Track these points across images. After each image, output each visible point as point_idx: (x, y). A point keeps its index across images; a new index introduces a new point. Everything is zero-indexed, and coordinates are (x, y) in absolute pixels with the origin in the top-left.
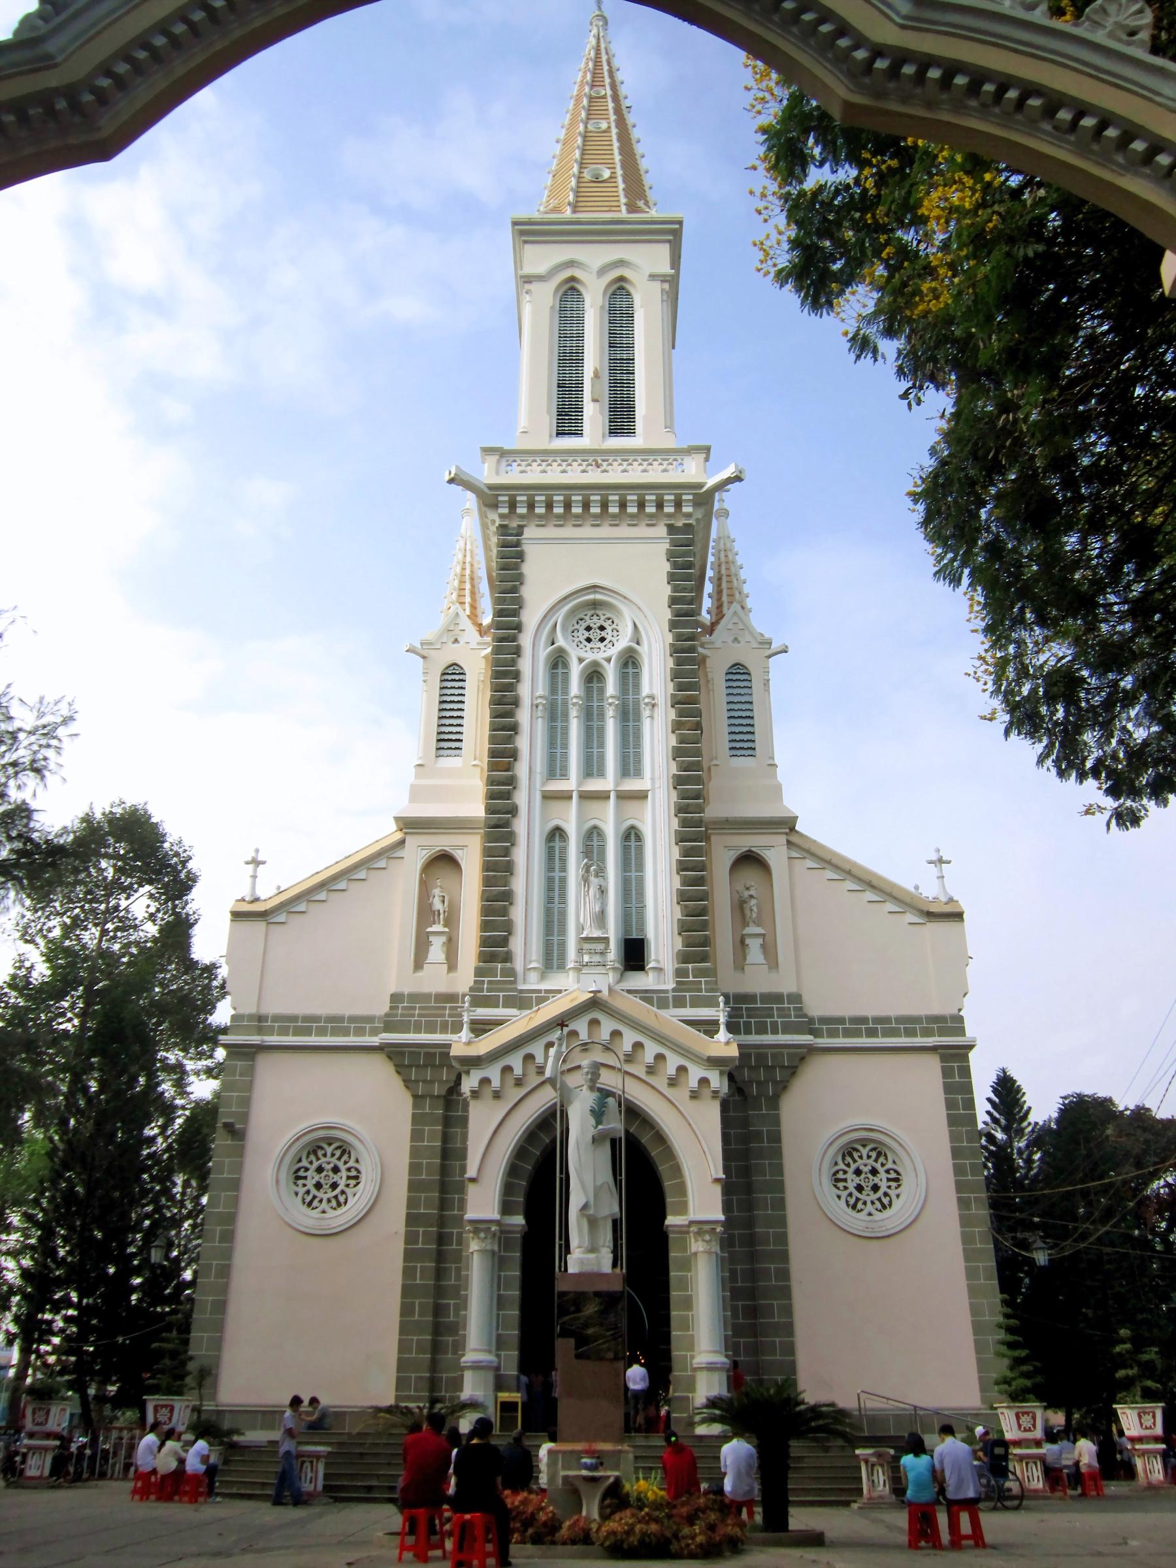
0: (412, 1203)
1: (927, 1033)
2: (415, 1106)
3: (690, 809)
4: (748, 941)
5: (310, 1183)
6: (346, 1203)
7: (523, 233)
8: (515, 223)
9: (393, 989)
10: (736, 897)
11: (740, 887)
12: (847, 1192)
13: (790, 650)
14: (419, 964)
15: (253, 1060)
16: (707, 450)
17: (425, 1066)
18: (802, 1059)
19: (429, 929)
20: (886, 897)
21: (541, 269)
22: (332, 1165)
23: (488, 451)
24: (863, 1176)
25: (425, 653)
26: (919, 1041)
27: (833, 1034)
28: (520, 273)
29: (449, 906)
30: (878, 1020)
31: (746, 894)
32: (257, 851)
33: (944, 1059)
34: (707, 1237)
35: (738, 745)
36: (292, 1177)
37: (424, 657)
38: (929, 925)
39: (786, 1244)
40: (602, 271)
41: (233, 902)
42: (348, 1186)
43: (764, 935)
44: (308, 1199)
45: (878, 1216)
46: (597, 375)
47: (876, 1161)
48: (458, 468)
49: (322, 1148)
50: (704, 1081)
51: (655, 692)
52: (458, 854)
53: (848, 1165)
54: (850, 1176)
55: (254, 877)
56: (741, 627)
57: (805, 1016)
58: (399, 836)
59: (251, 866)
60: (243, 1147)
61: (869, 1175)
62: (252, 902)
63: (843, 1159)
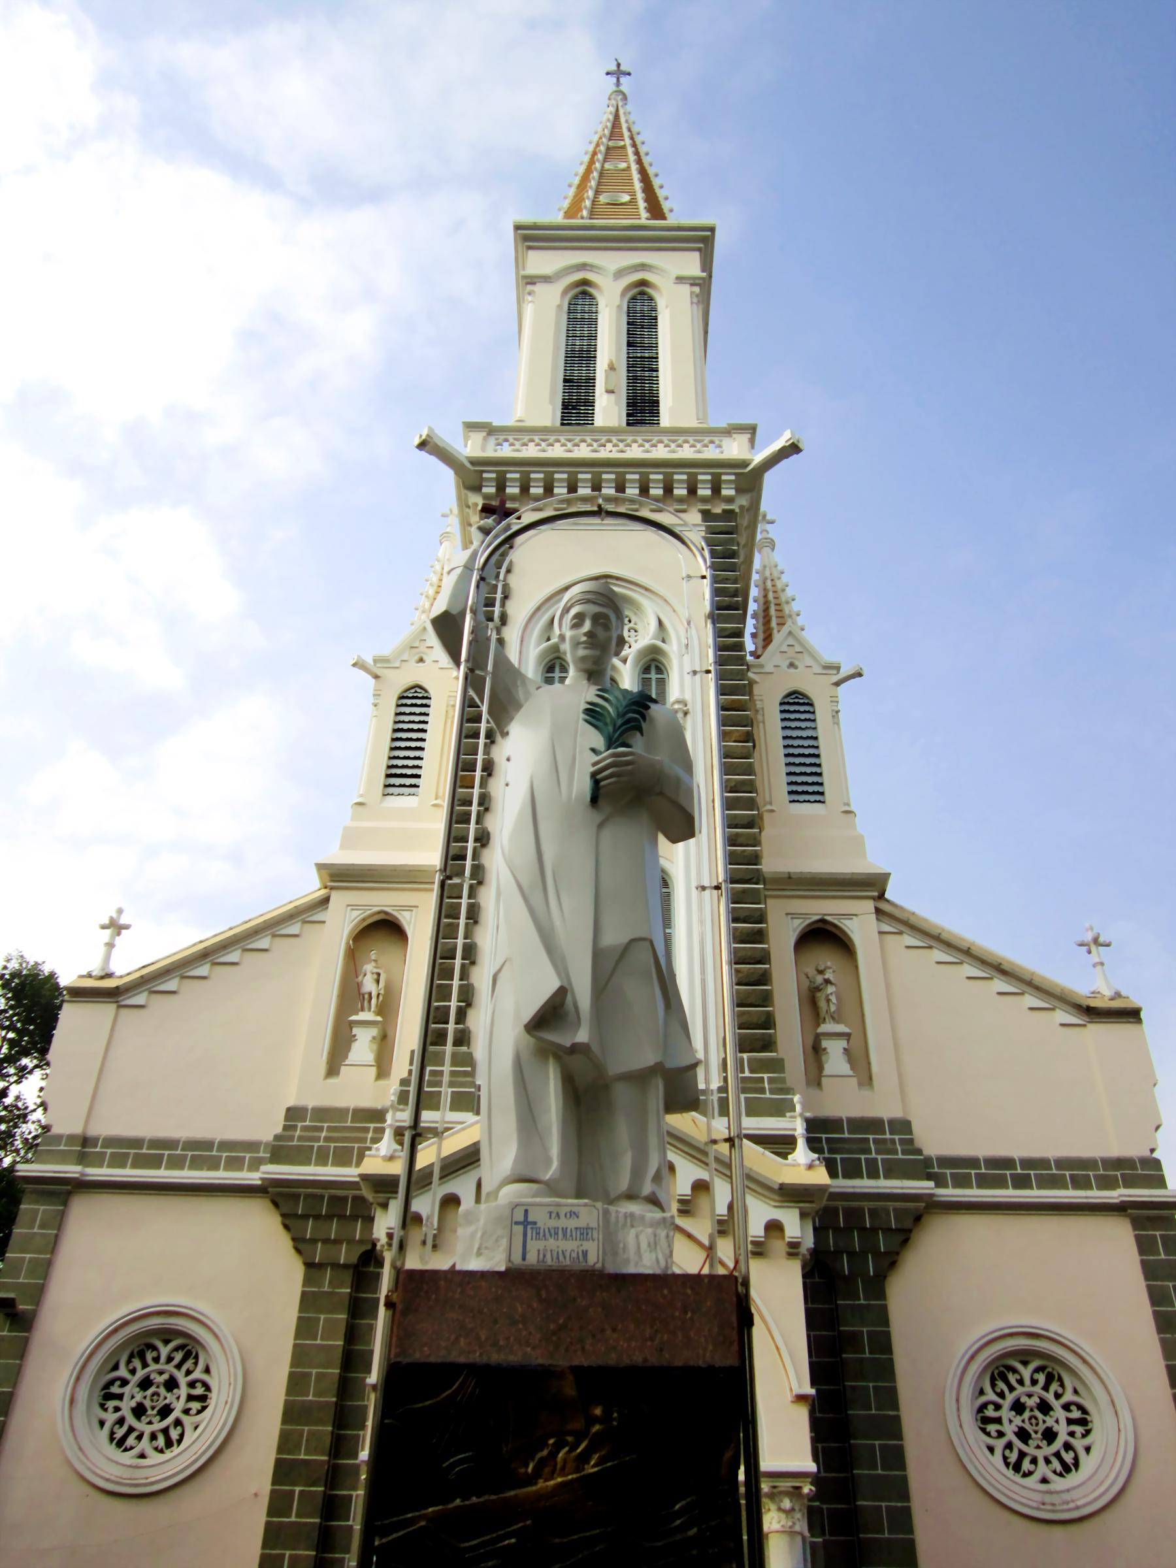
0: (286, 1442)
1: (1107, 1183)
2: (307, 1281)
3: (740, 840)
4: (825, 1043)
5: (126, 1406)
6: (180, 1441)
7: (526, 238)
8: (518, 227)
9: (291, 1103)
10: (806, 984)
11: (811, 971)
12: (1003, 1441)
13: (865, 672)
14: (333, 1070)
15: (65, 1203)
16: (752, 429)
17: (329, 1217)
18: (918, 1219)
19: (353, 1018)
20: (1025, 988)
21: (547, 270)
22: (166, 1376)
23: (471, 427)
24: (1027, 1414)
25: (379, 672)
26: (1096, 1195)
27: (962, 1182)
28: (522, 273)
29: (387, 988)
30: (1028, 1163)
31: (819, 979)
32: (120, 911)
33: (1137, 1223)
34: (787, 1503)
35: (800, 788)
36: (97, 1399)
37: (376, 677)
38: (1089, 1025)
39: (911, 1530)
40: (619, 274)
41: (76, 977)
42: (187, 1412)
43: (847, 1036)
44: (120, 1433)
45: (1058, 1483)
46: (612, 368)
47: (1046, 1388)
48: (430, 429)
49: (154, 1348)
50: (774, 1227)
51: (688, 697)
52: (406, 919)
53: (1001, 1395)
54: (1005, 1413)
55: (110, 945)
56: (798, 649)
57: (919, 1152)
58: (324, 892)
59: (108, 932)
60: (26, 1341)
61: (1037, 1413)
62: (102, 978)
63: (993, 1385)
